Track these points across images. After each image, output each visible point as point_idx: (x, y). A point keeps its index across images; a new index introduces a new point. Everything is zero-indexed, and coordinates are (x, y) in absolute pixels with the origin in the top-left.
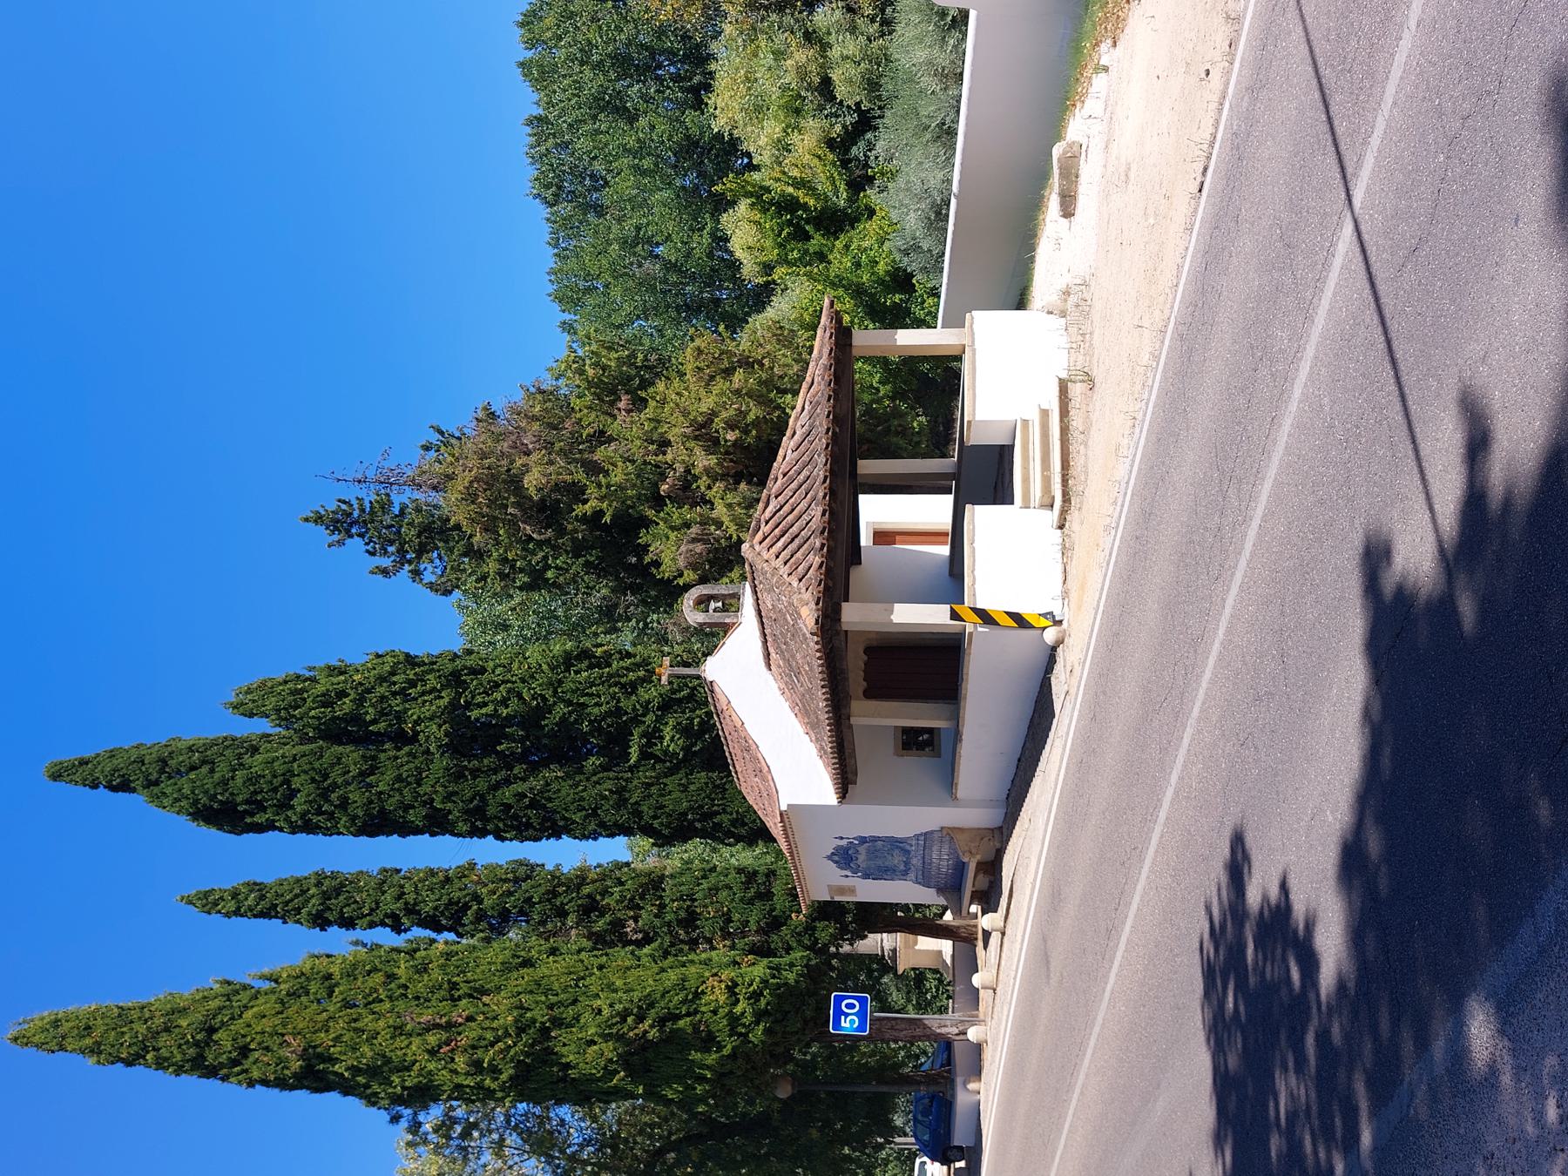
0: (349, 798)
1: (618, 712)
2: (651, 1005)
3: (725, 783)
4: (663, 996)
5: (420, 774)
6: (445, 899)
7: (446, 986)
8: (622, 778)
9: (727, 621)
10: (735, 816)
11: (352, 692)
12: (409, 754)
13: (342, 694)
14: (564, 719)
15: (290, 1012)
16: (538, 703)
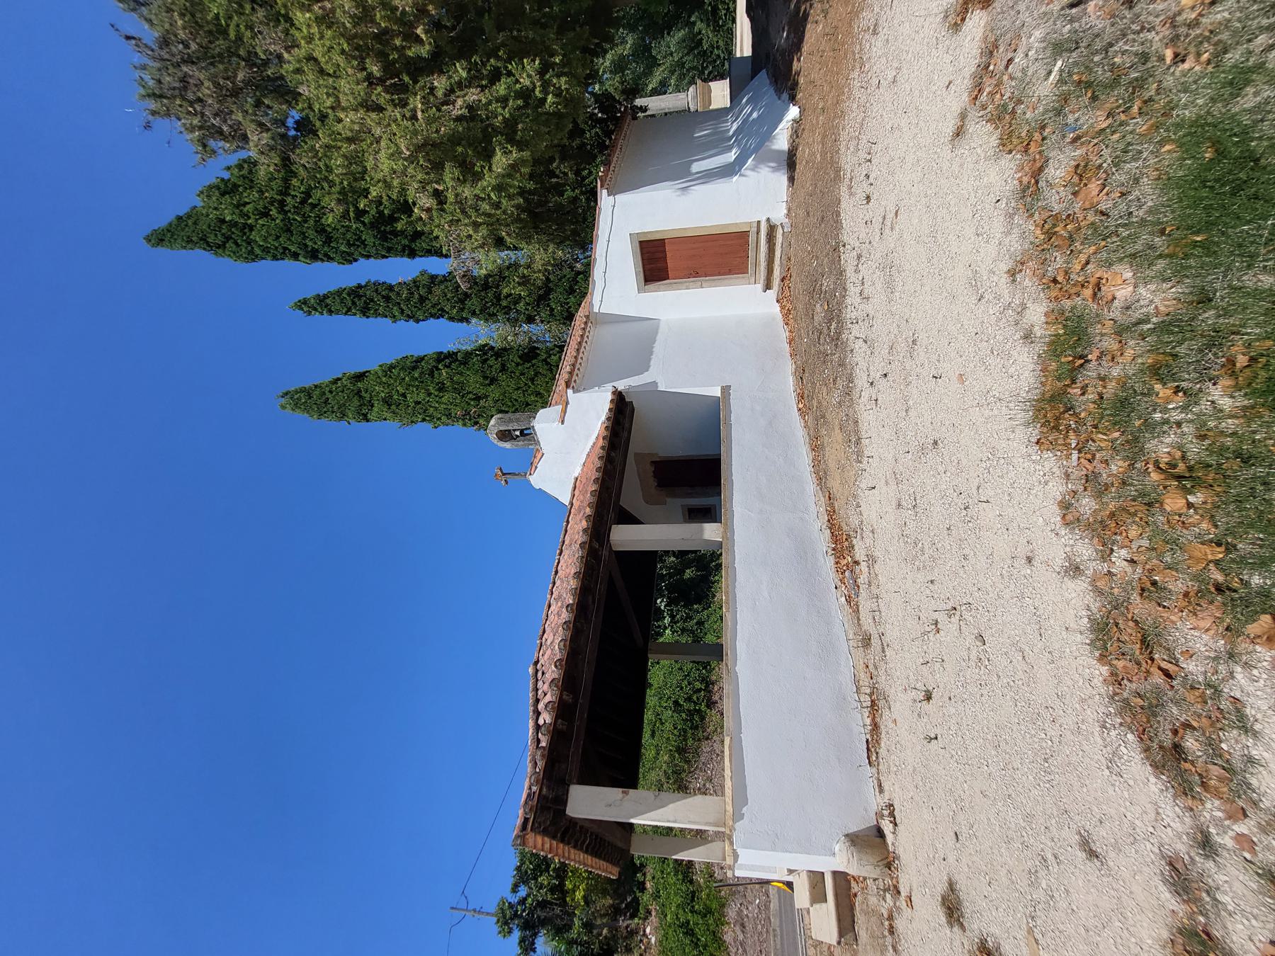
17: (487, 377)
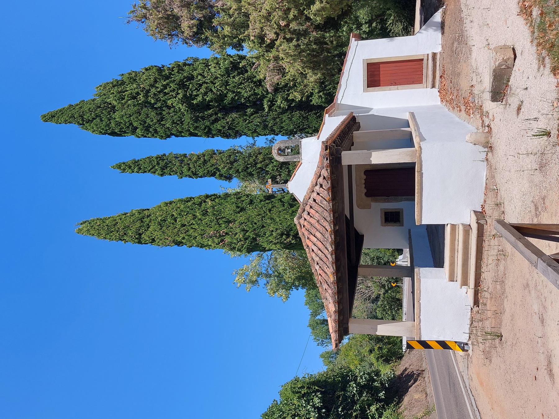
0: (157, 130)
1: (256, 94)
3: (308, 116)
5: (181, 119)
7: (215, 220)
9: (295, 160)
10: (314, 128)
11: (142, 93)
12: (174, 112)
13: (138, 94)
15: (164, 228)
17: (239, 207)
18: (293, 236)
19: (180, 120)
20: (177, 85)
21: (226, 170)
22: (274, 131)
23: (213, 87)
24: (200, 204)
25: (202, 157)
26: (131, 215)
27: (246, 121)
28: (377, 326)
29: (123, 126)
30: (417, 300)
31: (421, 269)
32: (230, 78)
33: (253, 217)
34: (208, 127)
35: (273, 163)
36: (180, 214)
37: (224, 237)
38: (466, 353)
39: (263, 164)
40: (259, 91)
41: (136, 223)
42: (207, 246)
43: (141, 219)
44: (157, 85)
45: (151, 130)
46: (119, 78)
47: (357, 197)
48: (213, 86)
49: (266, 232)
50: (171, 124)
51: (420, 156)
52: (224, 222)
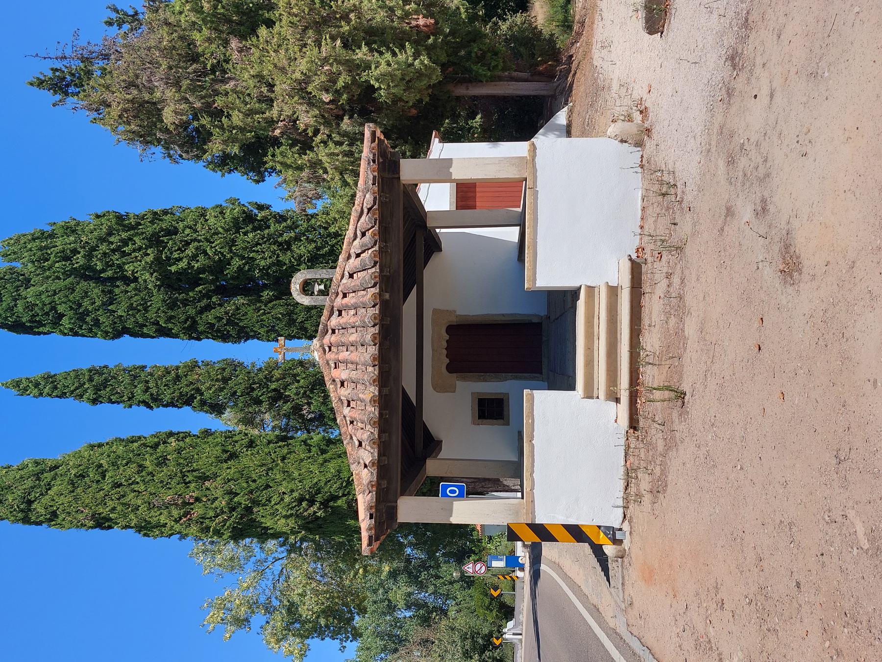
1: (279, 263)
2: (318, 492)
4: (326, 484)
5: (146, 303)
6: (177, 394)
7: (179, 475)
8: (290, 304)
11: (82, 251)
12: (135, 289)
13: (75, 252)
14: (240, 269)
15: (79, 490)
16: (220, 258)
17: (227, 452)
18: (321, 503)
19: (143, 304)
20: (147, 239)
21: (213, 393)
22: (306, 330)
23: (209, 247)
24: (155, 446)
25: (173, 370)
26: (20, 468)
27: (258, 312)
28: (453, 504)
29: (38, 311)
30: (527, 437)
31: (537, 393)
32: (240, 235)
33: (251, 469)
34: (192, 318)
35: (298, 381)
36: (114, 464)
37: (192, 506)
38: (618, 547)
39: (281, 384)
40: (285, 258)
41: (25, 481)
42: (157, 527)
43: (38, 473)
44: (112, 239)
45: (88, 319)
46: (48, 229)
47: (432, 371)
48: (208, 245)
49: (272, 497)
50: (126, 310)
51: (533, 160)
52: (196, 477)
